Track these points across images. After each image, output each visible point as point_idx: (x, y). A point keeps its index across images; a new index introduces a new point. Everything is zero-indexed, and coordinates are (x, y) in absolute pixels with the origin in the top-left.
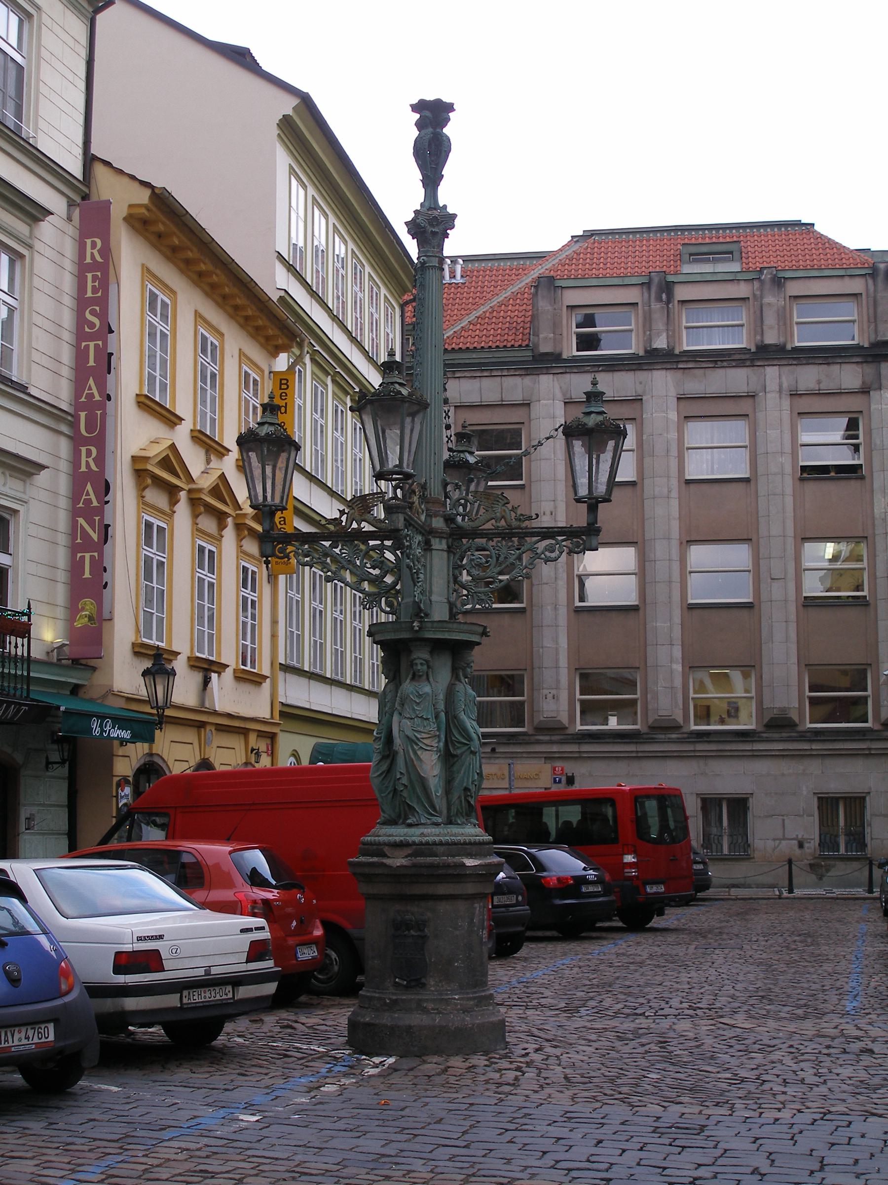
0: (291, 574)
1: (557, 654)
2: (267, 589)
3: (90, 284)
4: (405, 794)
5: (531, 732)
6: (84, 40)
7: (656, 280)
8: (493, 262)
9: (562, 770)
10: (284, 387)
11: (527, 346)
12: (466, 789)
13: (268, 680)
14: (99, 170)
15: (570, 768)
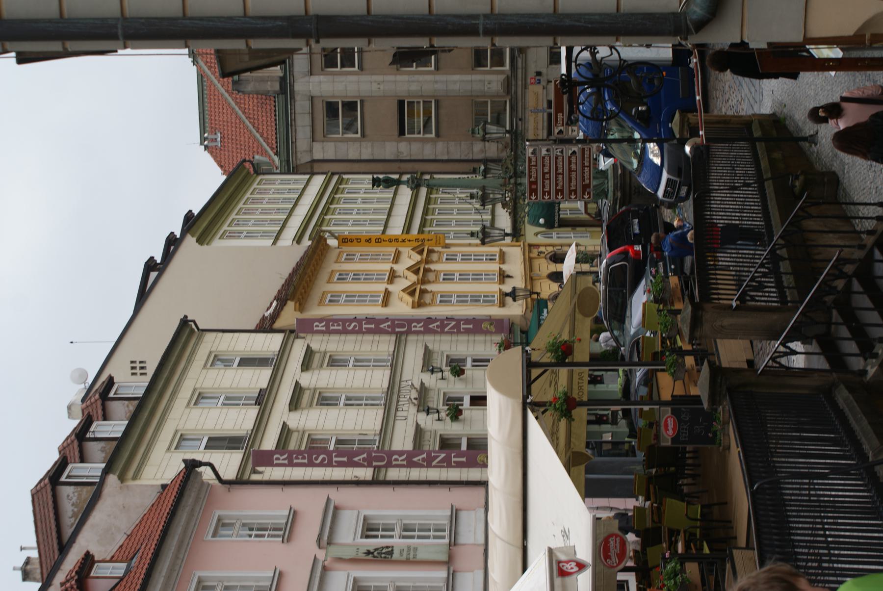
0: (445, 237)
1: (463, 81)
2: (453, 249)
4: (598, 192)
5: (509, 97)
6: (214, 334)
8: (205, 114)
9: (532, 78)
10: (346, 240)
11: (275, 97)
12: (596, 172)
13: (501, 248)
15: (531, 74)
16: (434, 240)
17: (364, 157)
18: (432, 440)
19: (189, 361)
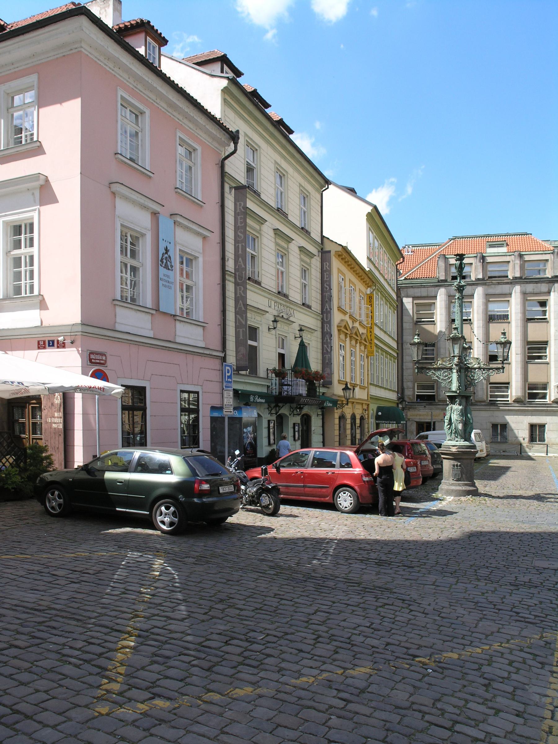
3: (239, 221)
7: (479, 255)
14: (325, 240)
16: (371, 350)
17: (404, 325)
18: (255, 320)
19: (304, 177)
